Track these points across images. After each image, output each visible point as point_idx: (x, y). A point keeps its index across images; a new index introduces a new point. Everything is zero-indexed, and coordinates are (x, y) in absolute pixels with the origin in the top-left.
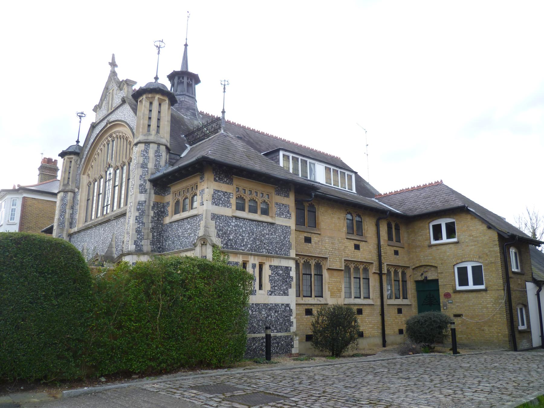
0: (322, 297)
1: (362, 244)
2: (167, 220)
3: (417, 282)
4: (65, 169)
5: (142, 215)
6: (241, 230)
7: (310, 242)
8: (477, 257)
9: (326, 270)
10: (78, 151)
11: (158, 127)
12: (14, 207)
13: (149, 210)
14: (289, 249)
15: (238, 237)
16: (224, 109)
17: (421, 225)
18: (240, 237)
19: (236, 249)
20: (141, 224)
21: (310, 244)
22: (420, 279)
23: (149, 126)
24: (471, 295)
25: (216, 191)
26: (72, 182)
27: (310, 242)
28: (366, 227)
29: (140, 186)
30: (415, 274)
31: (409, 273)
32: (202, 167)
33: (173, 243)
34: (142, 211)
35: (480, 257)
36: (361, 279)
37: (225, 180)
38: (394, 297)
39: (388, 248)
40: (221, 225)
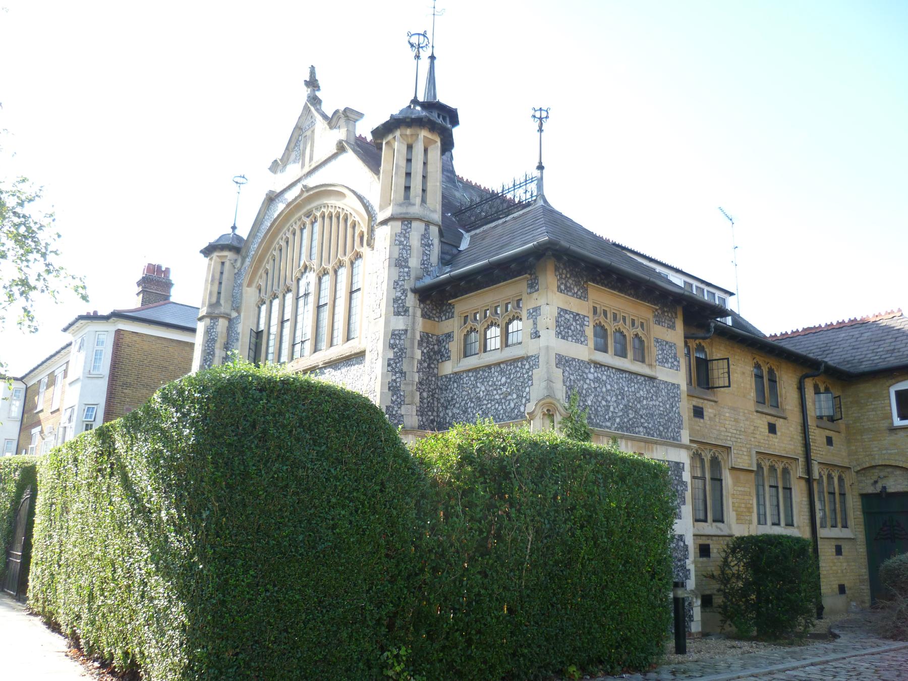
0: (723, 522)
1: (779, 423)
2: (448, 368)
3: (865, 497)
4: (213, 276)
6: (604, 390)
10: (235, 244)
11: (424, 191)
12: (99, 348)
13: (413, 347)
14: (679, 428)
15: (600, 402)
16: (540, 163)
17: (873, 390)
18: (604, 403)
19: (597, 425)
21: (702, 420)
22: (870, 490)
25: (562, 311)
26: (226, 302)
28: (784, 391)
29: (395, 300)
30: (860, 482)
31: (849, 479)
34: (401, 350)
36: (780, 490)
39: (818, 431)
40: (572, 378)
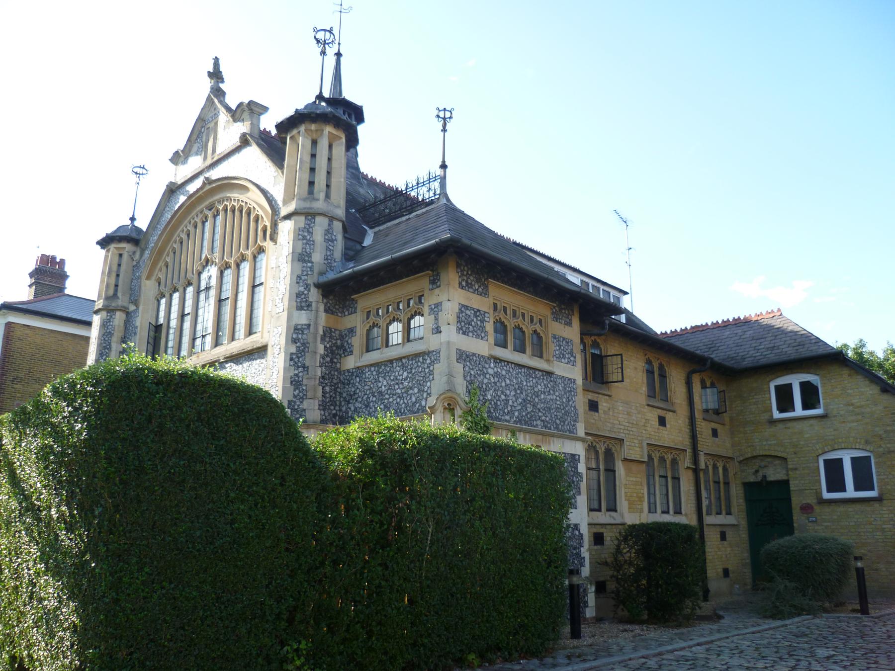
0: (616, 511)
1: (669, 416)
2: (350, 363)
5: (303, 351)
6: (503, 384)
7: (597, 411)
8: (863, 442)
9: (620, 462)
10: (134, 235)
13: (315, 341)
14: (575, 421)
15: (500, 397)
16: (444, 162)
18: (503, 397)
20: (300, 369)
22: (752, 479)
23: (311, 183)
24: (851, 508)
25: (463, 307)
26: (124, 294)
27: (597, 411)
28: (673, 385)
31: (733, 469)
32: (426, 263)
33: (367, 406)
34: (303, 344)
35: (867, 442)
36: (670, 479)
37: (477, 287)
38: (714, 512)
39: (704, 424)
40: (472, 372)
